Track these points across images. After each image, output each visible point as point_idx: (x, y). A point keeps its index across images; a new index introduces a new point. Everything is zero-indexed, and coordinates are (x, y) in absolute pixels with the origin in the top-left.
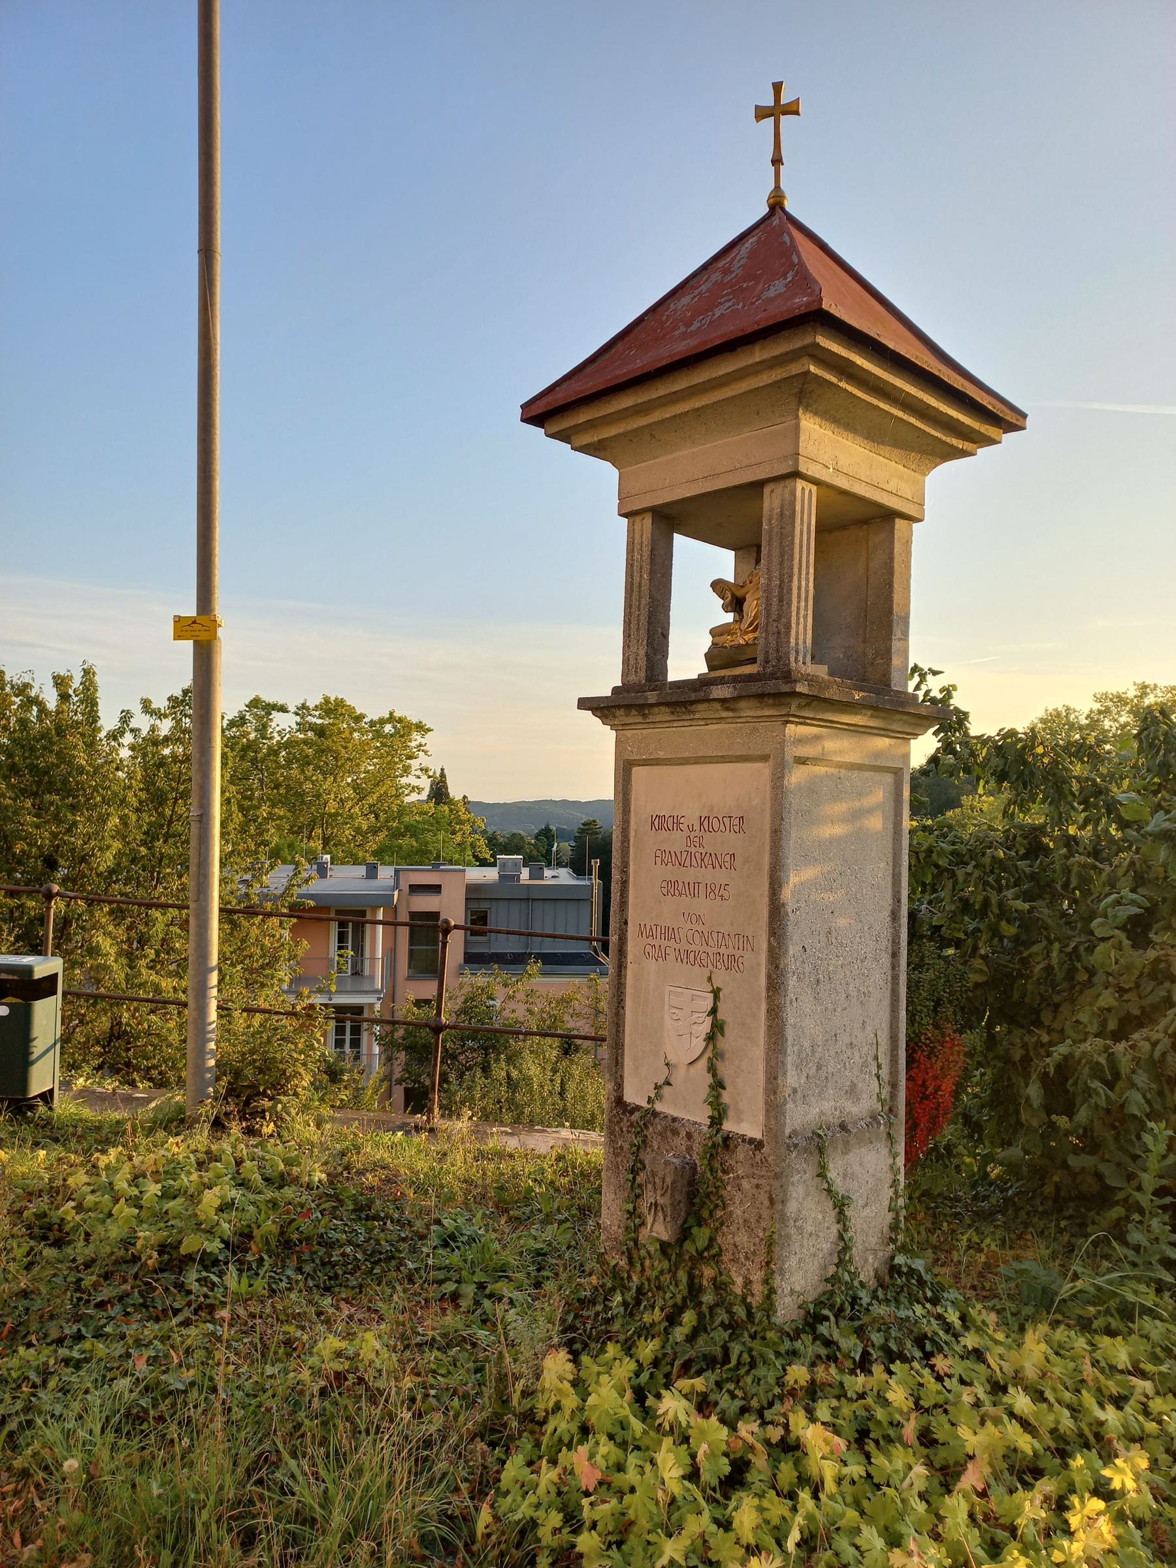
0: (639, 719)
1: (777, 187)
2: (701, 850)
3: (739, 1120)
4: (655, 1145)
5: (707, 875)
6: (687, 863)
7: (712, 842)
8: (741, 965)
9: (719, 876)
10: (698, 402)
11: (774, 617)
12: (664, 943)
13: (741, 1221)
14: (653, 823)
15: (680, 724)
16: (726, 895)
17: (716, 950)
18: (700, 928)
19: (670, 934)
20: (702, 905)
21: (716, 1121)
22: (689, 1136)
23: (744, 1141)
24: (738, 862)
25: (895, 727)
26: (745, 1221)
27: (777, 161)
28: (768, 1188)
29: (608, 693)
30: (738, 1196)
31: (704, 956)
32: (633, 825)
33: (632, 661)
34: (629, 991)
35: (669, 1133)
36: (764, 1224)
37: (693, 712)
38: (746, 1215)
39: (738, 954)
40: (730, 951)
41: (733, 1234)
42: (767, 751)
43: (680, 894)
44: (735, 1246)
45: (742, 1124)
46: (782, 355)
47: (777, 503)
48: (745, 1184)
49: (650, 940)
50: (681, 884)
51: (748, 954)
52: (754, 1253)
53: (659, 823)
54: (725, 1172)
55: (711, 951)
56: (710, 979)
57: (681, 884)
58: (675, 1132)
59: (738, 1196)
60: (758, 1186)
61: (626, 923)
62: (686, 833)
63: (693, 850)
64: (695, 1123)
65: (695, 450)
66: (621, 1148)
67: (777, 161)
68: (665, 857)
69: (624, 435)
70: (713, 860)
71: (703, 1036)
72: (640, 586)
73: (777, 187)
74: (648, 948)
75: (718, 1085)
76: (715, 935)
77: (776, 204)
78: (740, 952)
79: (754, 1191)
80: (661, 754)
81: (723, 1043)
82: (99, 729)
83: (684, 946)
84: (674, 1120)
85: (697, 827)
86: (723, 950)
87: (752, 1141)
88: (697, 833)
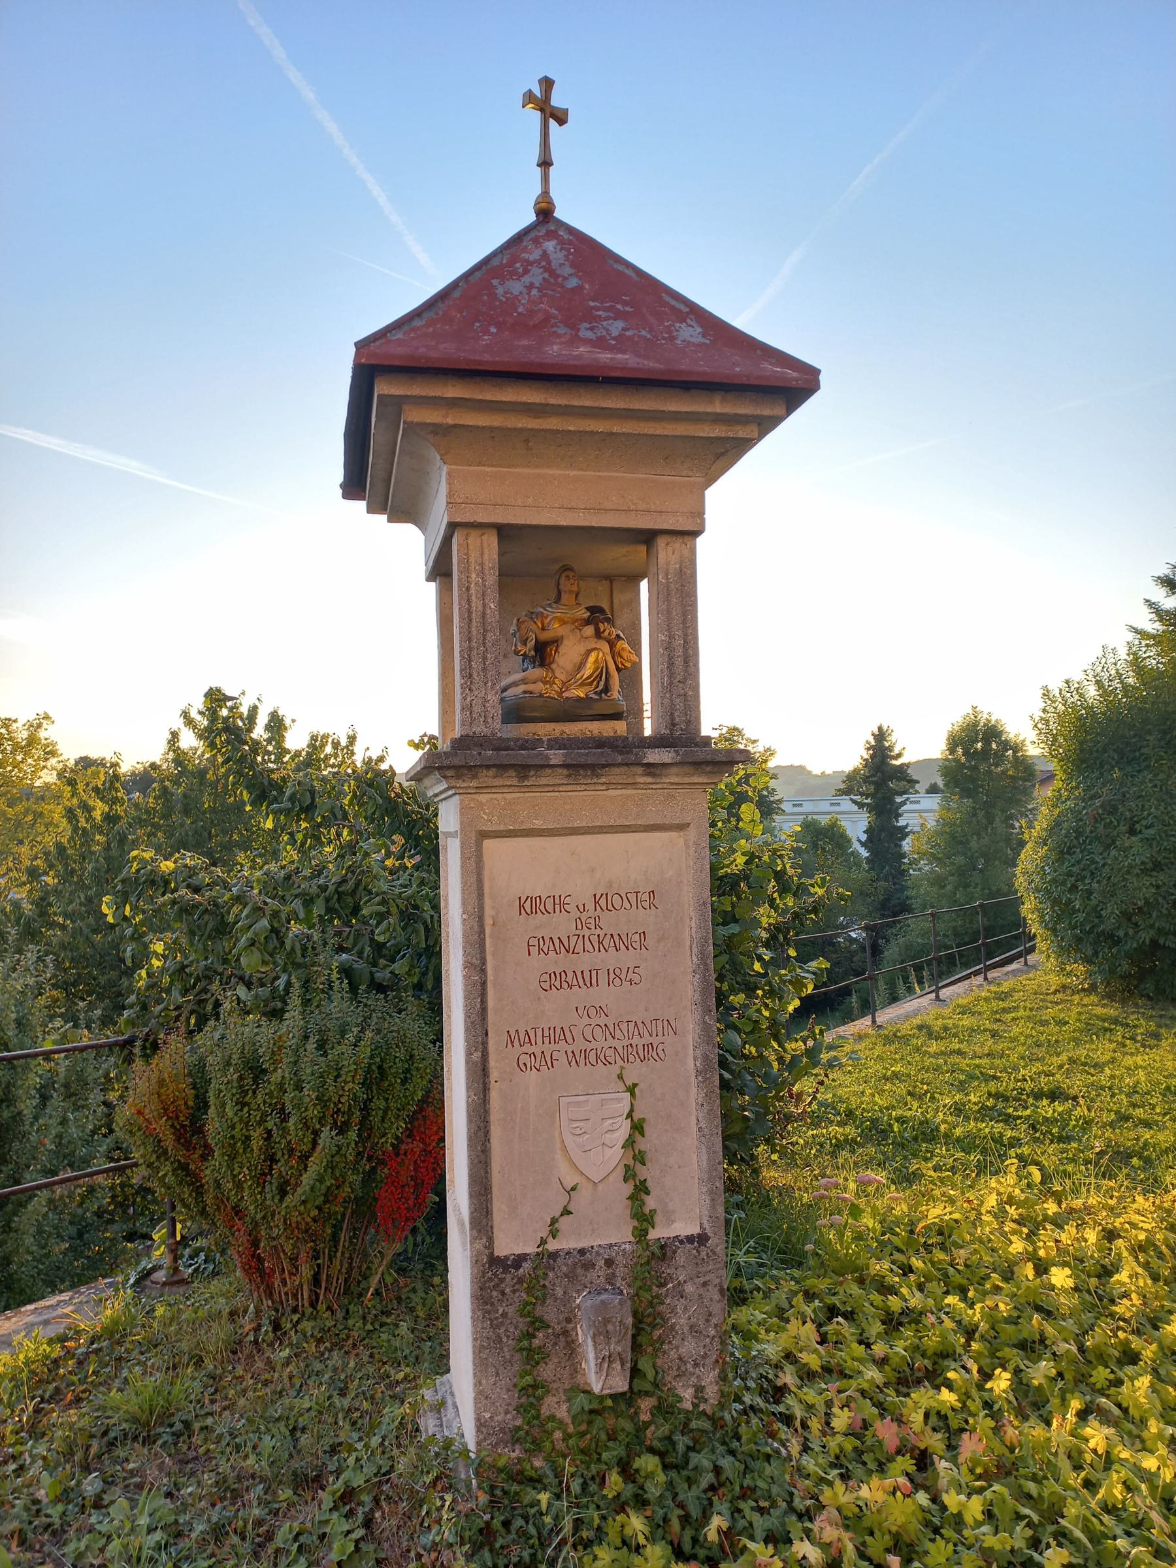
0: (515, 782)
1: (546, 192)
2: (598, 931)
3: (670, 1222)
4: (559, 1292)
5: (610, 959)
6: (579, 948)
7: (610, 923)
8: (661, 1053)
9: (627, 958)
10: (600, 426)
11: (679, 678)
12: (548, 1048)
13: (686, 1329)
14: (521, 907)
15: (570, 788)
16: (636, 978)
17: (626, 1042)
18: (602, 1020)
19: (559, 1035)
20: (603, 995)
21: (641, 1234)
22: (609, 1263)
23: (681, 1242)
24: (650, 941)
25: (544, 781)
26: (691, 1327)
27: (545, 163)
28: (717, 1281)
29: (817, 771)
30: (680, 1305)
31: (610, 1052)
32: (489, 912)
33: (477, 709)
34: (494, 1117)
35: (579, 1271)
36: (714, 1321)
37: (598, 776)
38: (693, 1320)
39: (656, 1041)
40: (647, 1039)
41: (677, 1348)
42: (688, 820)
43: (570, 986)
44: (680, 1359)
45: (675, 1225)
46: (686, 413)
47: (674, 559)
48: (689, 1288)
49: (527, 1048)
50: (571, 975)
51: (670, 1039)
52: (705, 1356)
53: (530, 905)
54: (662, 1285)
55: (618, 1045)
56: (620, 1077)
57: (571, 975)
58: (589, 1266)
59: (680, 1305)
60: (705, 1284)
61: (487, 1034)
62: (575, 913)
63: (586, 933)
64: (611, 1246)
65: (572, 473)
66: (504, 1315)
67: (545, 163)
68: (541, 945)
69: (491, 429)
70: (619, 942)
71: (621, 1143)
72: (484, 614)
73: (546, 192)
74: (524, 1059)
75: (641, 1189)
76: (624, 1026)
77: (545, 211)
78: (660, 1038)
79: (701, 1291)
80: (538, 824)
81: (642, 1144)
82: (903, 833)
83: (581, 1044)
84: (582, 1252)
85: (590, 906)
86: (636, 1040)
87: (690, 1239)
88: (591, 913)
